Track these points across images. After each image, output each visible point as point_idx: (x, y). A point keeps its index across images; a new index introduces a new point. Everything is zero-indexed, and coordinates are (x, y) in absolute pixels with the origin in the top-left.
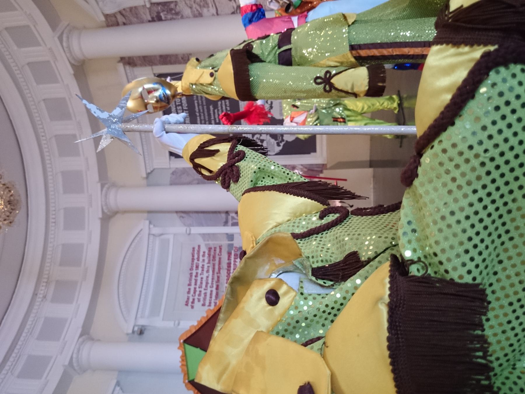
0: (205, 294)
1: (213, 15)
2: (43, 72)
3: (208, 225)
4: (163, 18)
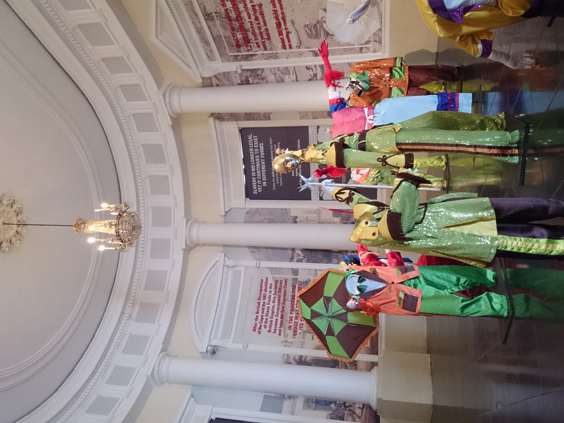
0: (271, 321)
1: (293, 81)
2: (145, 122)
3: (275, 261)
4: (251, 82)
